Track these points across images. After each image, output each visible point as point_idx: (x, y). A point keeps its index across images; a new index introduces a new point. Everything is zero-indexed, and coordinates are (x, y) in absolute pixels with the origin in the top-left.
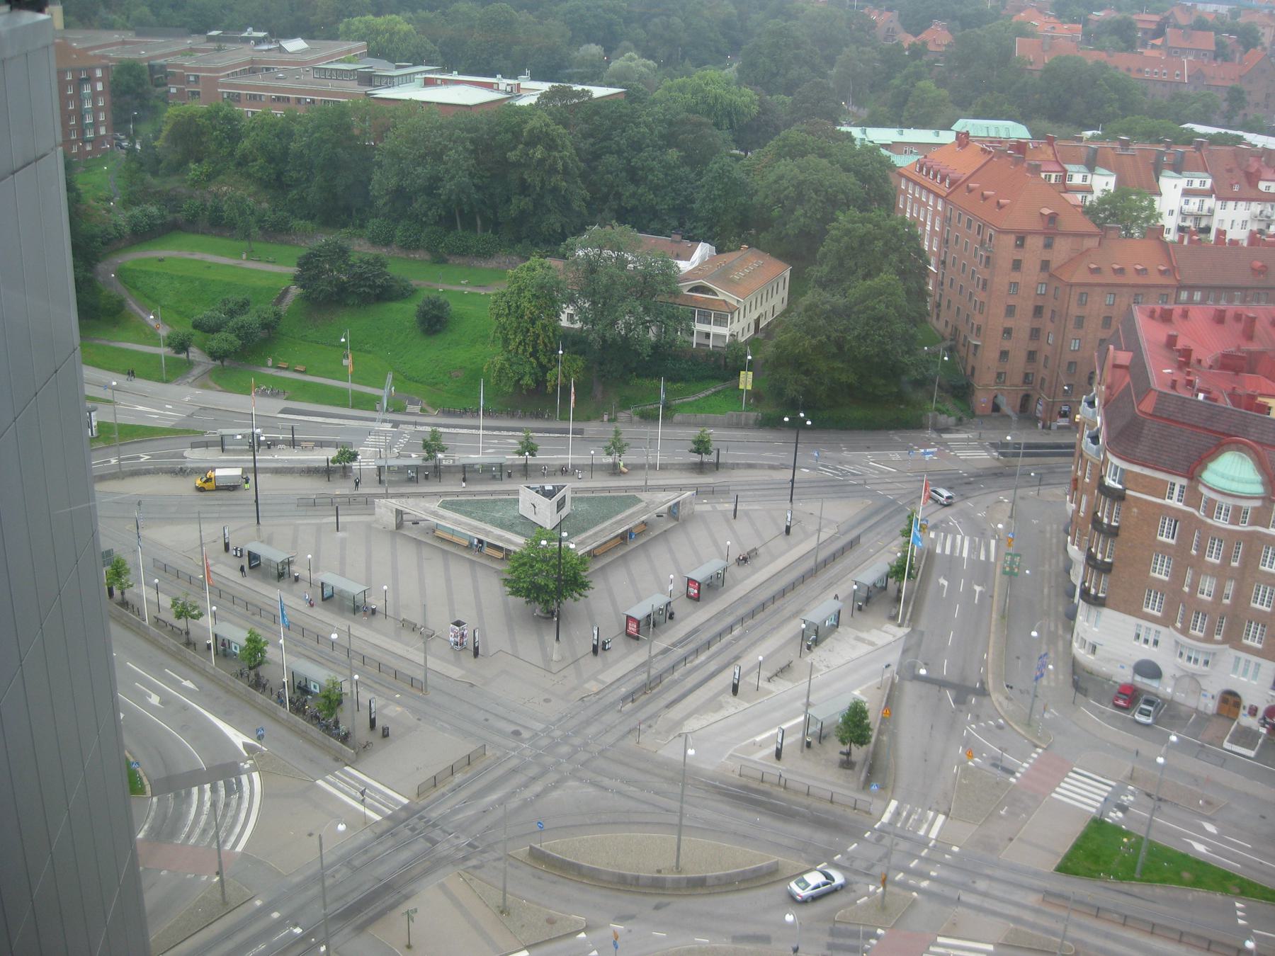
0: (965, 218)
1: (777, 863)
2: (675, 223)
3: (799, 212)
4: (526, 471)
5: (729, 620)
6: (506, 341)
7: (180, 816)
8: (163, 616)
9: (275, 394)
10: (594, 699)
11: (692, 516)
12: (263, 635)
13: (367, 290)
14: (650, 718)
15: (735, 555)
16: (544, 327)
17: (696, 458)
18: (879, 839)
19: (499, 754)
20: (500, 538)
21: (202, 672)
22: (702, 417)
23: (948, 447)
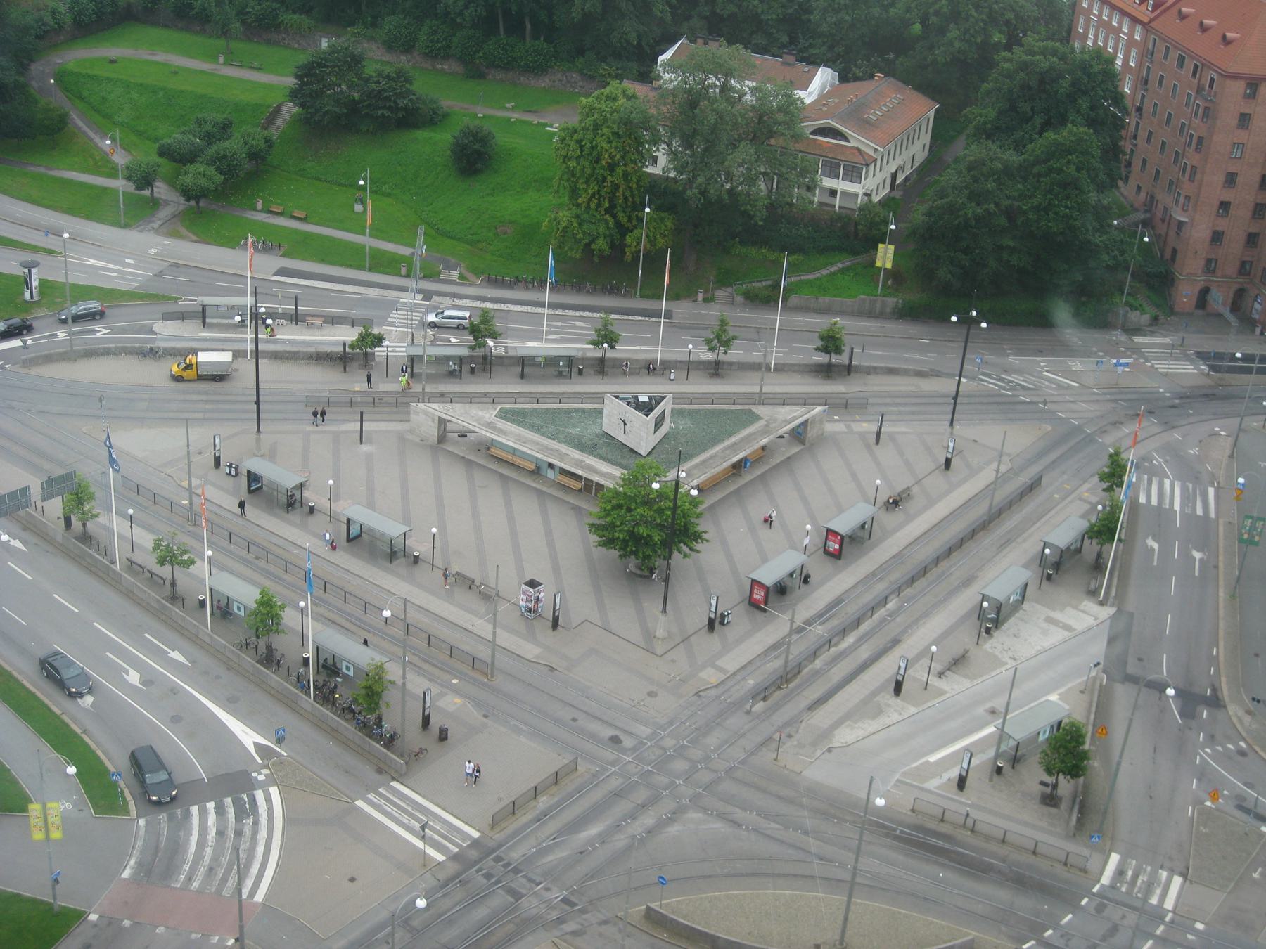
0: (1174, 55)
1: (973, 941)
2: (785, 39)
3: (953, 33)
4: (602, 367)
5: (880, 588)
6: (574, 192)
7: (176, 849)
8: (139, 558)
9: (267, 249)
10: (713, 692)
11: (822, 439)
12: (278, 592)
13: (386, 113)
14: (788, 724)
15: (883, 497)
16: (626, 175)
17: (822, 358)
18: (1100, 909)
19: (595, 769)
20: (579, 463)
21: (194, 639)
22: (825, 300)
23: (1142, 355)
